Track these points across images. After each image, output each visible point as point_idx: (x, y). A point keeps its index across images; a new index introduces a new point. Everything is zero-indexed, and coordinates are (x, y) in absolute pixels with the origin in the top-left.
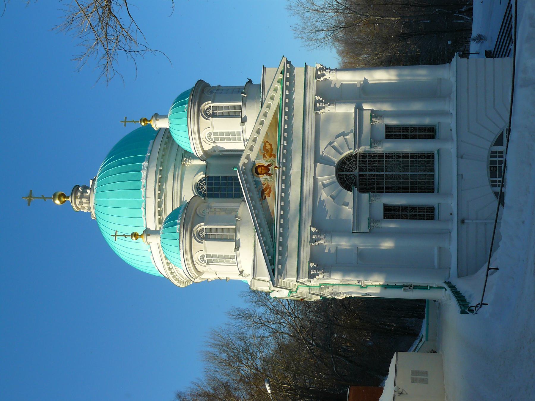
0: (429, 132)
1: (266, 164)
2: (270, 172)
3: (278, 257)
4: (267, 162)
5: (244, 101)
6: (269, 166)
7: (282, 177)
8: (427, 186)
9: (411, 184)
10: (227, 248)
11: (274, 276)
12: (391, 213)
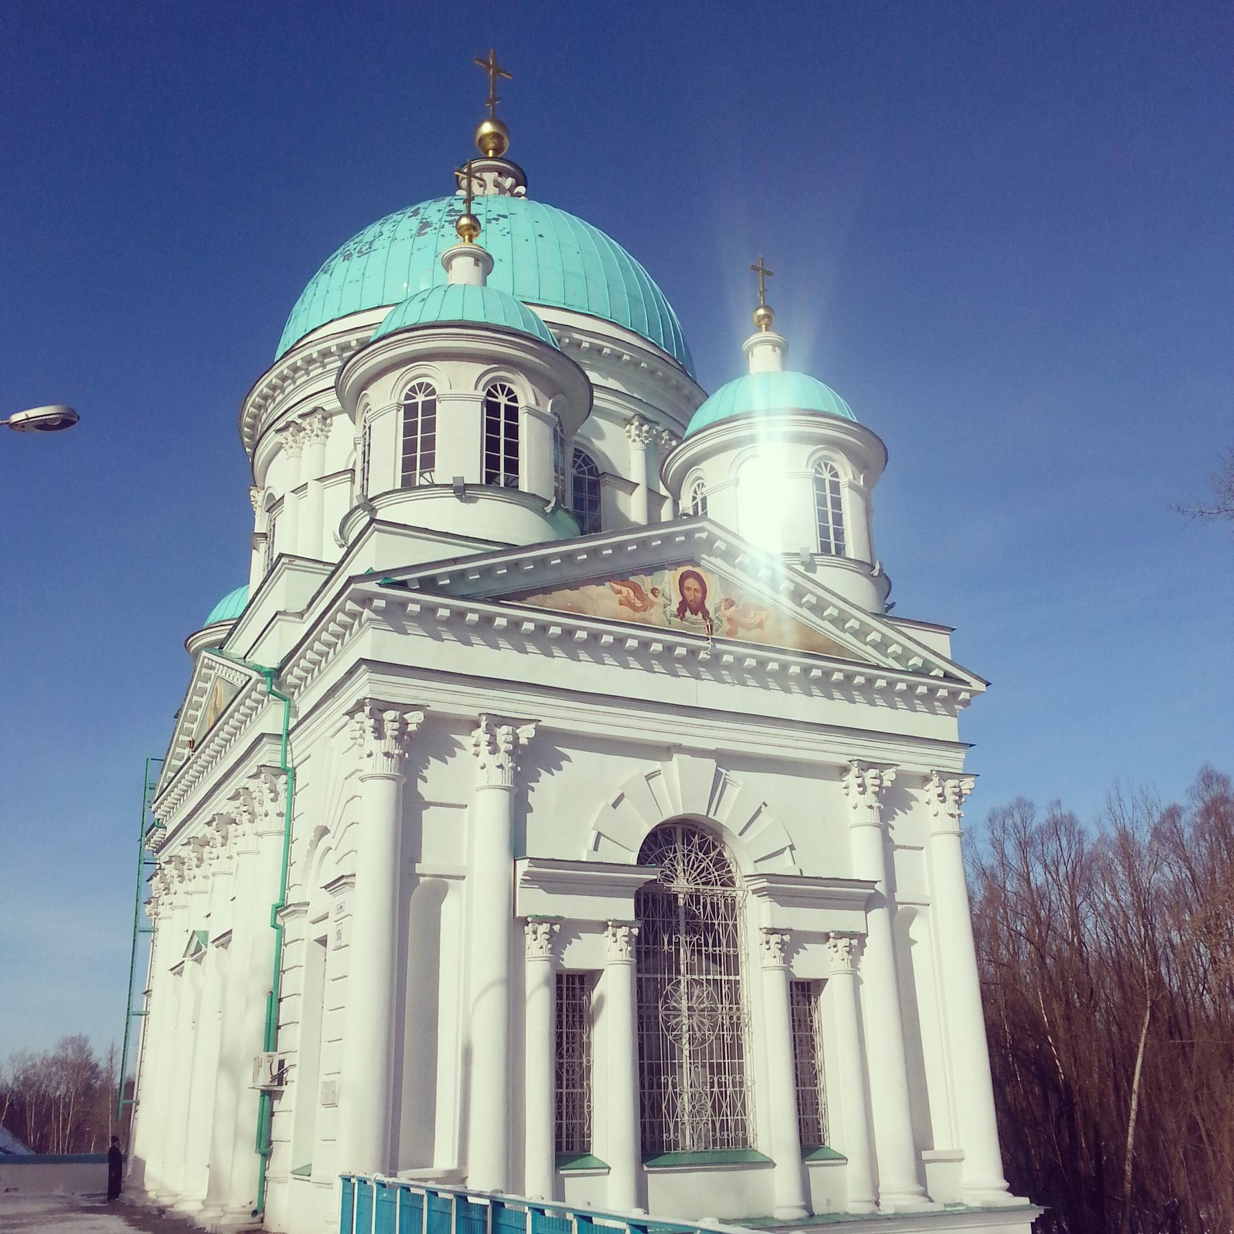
0: (811, 1140)
1: (709, 605)
2: (688, 614)
3: (797, 664)
4: (717, 610)
5: (864, 567)
6: (706, 615)
7: (682, 645)
8: (653, 1145)
9: (719, 1065)
10: (459, 445)
11: (968, 684)
12: (573, 991)
